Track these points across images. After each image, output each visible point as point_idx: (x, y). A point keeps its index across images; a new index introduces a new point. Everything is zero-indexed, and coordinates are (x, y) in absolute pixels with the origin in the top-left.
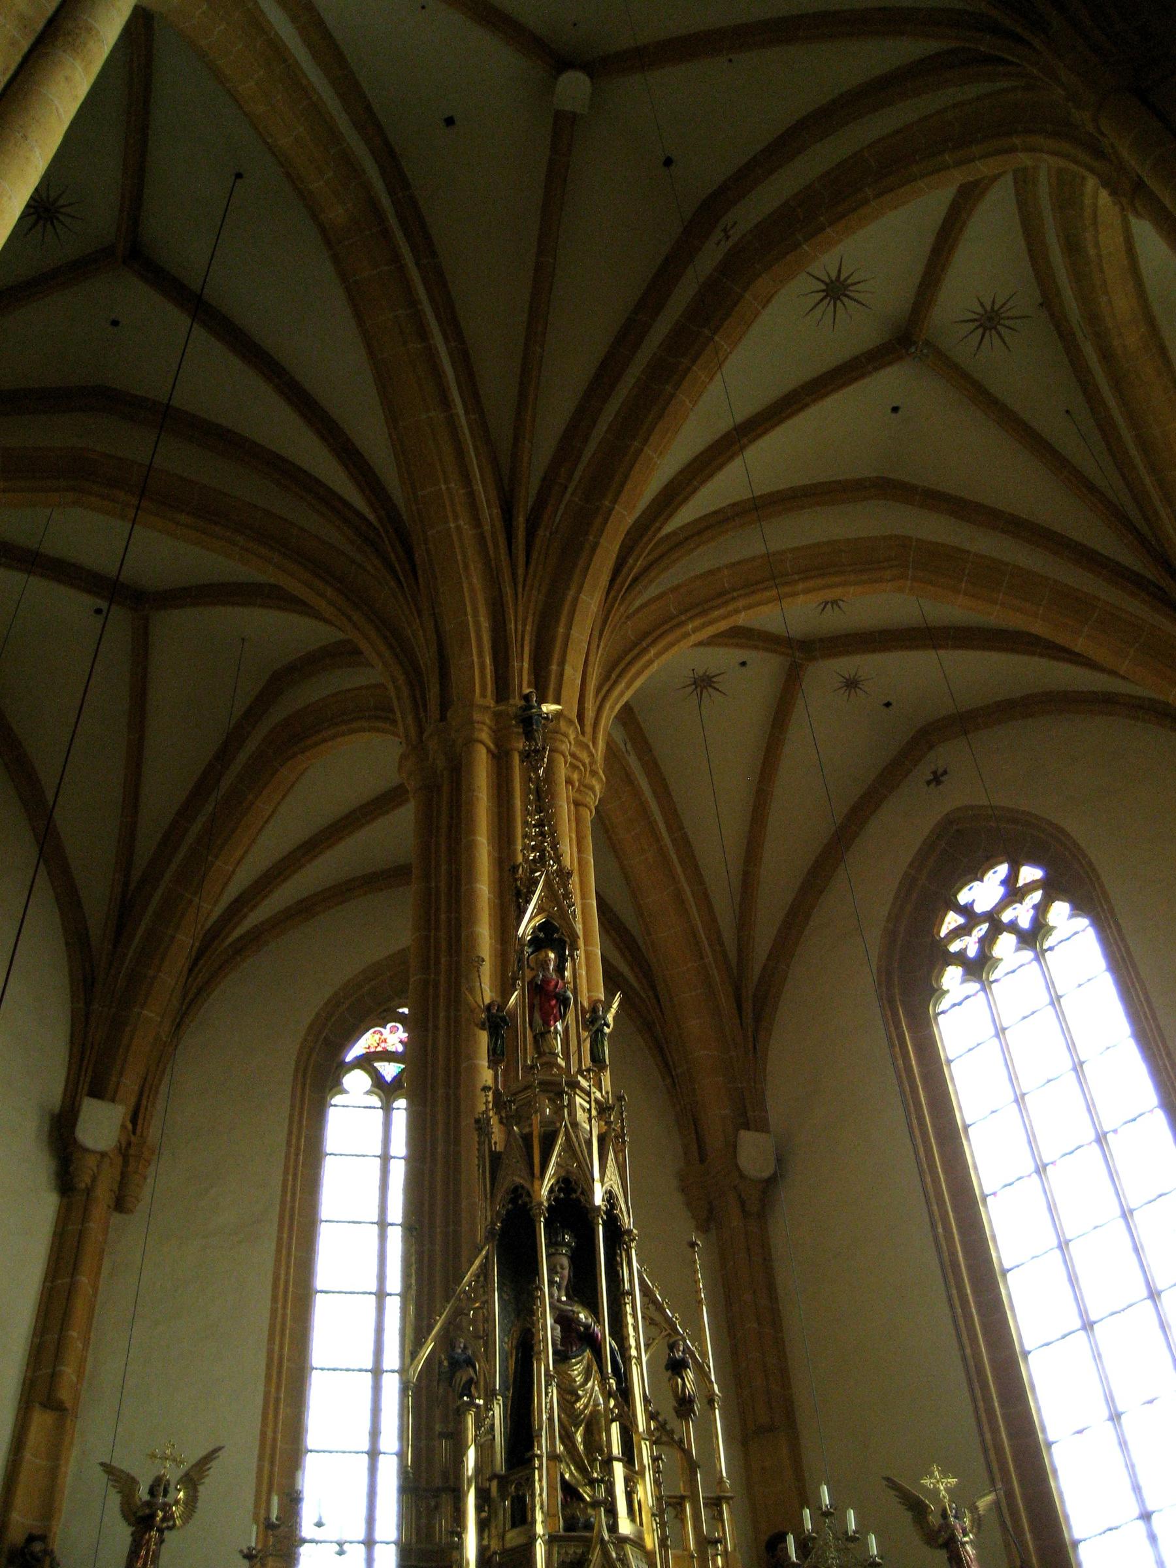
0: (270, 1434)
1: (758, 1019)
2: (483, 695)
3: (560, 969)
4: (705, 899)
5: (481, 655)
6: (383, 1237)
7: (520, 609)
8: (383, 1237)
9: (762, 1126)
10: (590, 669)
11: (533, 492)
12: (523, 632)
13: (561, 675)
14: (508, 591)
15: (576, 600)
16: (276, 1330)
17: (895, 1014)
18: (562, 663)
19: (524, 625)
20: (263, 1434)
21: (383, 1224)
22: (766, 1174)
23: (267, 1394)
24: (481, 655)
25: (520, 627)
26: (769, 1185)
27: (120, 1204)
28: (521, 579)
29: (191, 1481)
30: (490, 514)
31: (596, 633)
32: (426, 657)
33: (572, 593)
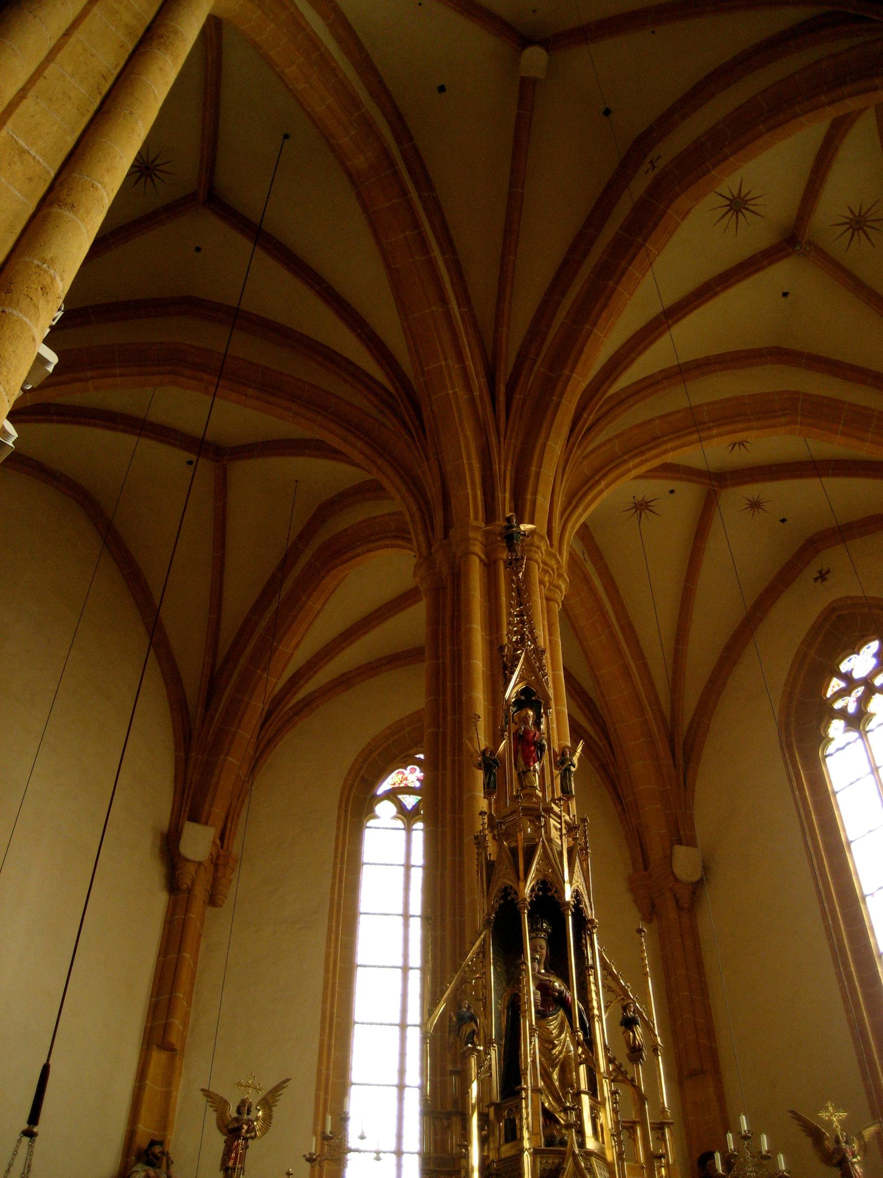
0: (324, 1072)
1: (687, 761)
2: (476, 519)
3: (537, 724)
4: (645, 668)
5: (474, 489)
6: (406, 925)
7: (503, 452)
8: (406, 925)
9: (691, 842)
10: (556, 498)
11: (511, 365)
12: (505, 471)
13: (534, 502)
14: (493, 439)
15: (544, 445)
16: (324, 1051)
17: (792, 756)
18: (535, 493)
19: (506, 466)
20: (319, 1072)
21: (406, 916)
22: (695, 879)
23: (322, 1041)
24: (474, 489)
25: (503, 467)
26: (697, 887)
27: (213, 900)
28: (502, 433)
29: (267, 1103)
30: (478, 382)
31: (560, 471)
32: (433, 491)
33: (541, 440)
